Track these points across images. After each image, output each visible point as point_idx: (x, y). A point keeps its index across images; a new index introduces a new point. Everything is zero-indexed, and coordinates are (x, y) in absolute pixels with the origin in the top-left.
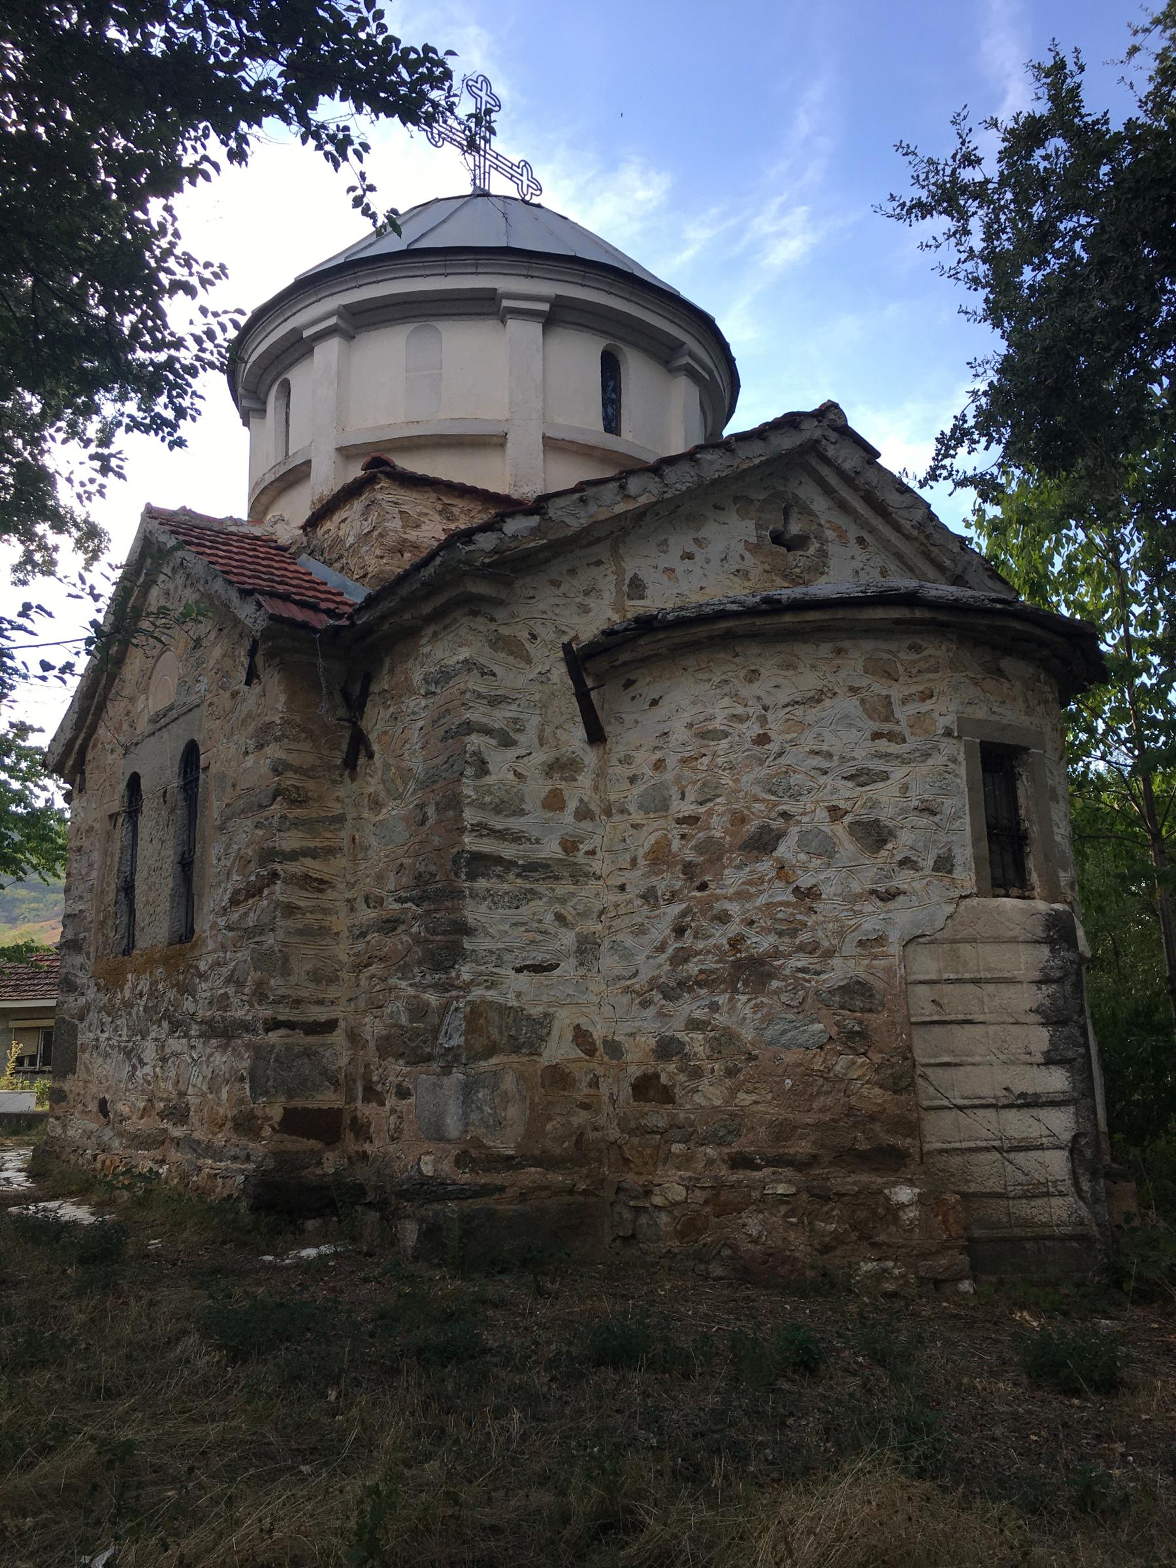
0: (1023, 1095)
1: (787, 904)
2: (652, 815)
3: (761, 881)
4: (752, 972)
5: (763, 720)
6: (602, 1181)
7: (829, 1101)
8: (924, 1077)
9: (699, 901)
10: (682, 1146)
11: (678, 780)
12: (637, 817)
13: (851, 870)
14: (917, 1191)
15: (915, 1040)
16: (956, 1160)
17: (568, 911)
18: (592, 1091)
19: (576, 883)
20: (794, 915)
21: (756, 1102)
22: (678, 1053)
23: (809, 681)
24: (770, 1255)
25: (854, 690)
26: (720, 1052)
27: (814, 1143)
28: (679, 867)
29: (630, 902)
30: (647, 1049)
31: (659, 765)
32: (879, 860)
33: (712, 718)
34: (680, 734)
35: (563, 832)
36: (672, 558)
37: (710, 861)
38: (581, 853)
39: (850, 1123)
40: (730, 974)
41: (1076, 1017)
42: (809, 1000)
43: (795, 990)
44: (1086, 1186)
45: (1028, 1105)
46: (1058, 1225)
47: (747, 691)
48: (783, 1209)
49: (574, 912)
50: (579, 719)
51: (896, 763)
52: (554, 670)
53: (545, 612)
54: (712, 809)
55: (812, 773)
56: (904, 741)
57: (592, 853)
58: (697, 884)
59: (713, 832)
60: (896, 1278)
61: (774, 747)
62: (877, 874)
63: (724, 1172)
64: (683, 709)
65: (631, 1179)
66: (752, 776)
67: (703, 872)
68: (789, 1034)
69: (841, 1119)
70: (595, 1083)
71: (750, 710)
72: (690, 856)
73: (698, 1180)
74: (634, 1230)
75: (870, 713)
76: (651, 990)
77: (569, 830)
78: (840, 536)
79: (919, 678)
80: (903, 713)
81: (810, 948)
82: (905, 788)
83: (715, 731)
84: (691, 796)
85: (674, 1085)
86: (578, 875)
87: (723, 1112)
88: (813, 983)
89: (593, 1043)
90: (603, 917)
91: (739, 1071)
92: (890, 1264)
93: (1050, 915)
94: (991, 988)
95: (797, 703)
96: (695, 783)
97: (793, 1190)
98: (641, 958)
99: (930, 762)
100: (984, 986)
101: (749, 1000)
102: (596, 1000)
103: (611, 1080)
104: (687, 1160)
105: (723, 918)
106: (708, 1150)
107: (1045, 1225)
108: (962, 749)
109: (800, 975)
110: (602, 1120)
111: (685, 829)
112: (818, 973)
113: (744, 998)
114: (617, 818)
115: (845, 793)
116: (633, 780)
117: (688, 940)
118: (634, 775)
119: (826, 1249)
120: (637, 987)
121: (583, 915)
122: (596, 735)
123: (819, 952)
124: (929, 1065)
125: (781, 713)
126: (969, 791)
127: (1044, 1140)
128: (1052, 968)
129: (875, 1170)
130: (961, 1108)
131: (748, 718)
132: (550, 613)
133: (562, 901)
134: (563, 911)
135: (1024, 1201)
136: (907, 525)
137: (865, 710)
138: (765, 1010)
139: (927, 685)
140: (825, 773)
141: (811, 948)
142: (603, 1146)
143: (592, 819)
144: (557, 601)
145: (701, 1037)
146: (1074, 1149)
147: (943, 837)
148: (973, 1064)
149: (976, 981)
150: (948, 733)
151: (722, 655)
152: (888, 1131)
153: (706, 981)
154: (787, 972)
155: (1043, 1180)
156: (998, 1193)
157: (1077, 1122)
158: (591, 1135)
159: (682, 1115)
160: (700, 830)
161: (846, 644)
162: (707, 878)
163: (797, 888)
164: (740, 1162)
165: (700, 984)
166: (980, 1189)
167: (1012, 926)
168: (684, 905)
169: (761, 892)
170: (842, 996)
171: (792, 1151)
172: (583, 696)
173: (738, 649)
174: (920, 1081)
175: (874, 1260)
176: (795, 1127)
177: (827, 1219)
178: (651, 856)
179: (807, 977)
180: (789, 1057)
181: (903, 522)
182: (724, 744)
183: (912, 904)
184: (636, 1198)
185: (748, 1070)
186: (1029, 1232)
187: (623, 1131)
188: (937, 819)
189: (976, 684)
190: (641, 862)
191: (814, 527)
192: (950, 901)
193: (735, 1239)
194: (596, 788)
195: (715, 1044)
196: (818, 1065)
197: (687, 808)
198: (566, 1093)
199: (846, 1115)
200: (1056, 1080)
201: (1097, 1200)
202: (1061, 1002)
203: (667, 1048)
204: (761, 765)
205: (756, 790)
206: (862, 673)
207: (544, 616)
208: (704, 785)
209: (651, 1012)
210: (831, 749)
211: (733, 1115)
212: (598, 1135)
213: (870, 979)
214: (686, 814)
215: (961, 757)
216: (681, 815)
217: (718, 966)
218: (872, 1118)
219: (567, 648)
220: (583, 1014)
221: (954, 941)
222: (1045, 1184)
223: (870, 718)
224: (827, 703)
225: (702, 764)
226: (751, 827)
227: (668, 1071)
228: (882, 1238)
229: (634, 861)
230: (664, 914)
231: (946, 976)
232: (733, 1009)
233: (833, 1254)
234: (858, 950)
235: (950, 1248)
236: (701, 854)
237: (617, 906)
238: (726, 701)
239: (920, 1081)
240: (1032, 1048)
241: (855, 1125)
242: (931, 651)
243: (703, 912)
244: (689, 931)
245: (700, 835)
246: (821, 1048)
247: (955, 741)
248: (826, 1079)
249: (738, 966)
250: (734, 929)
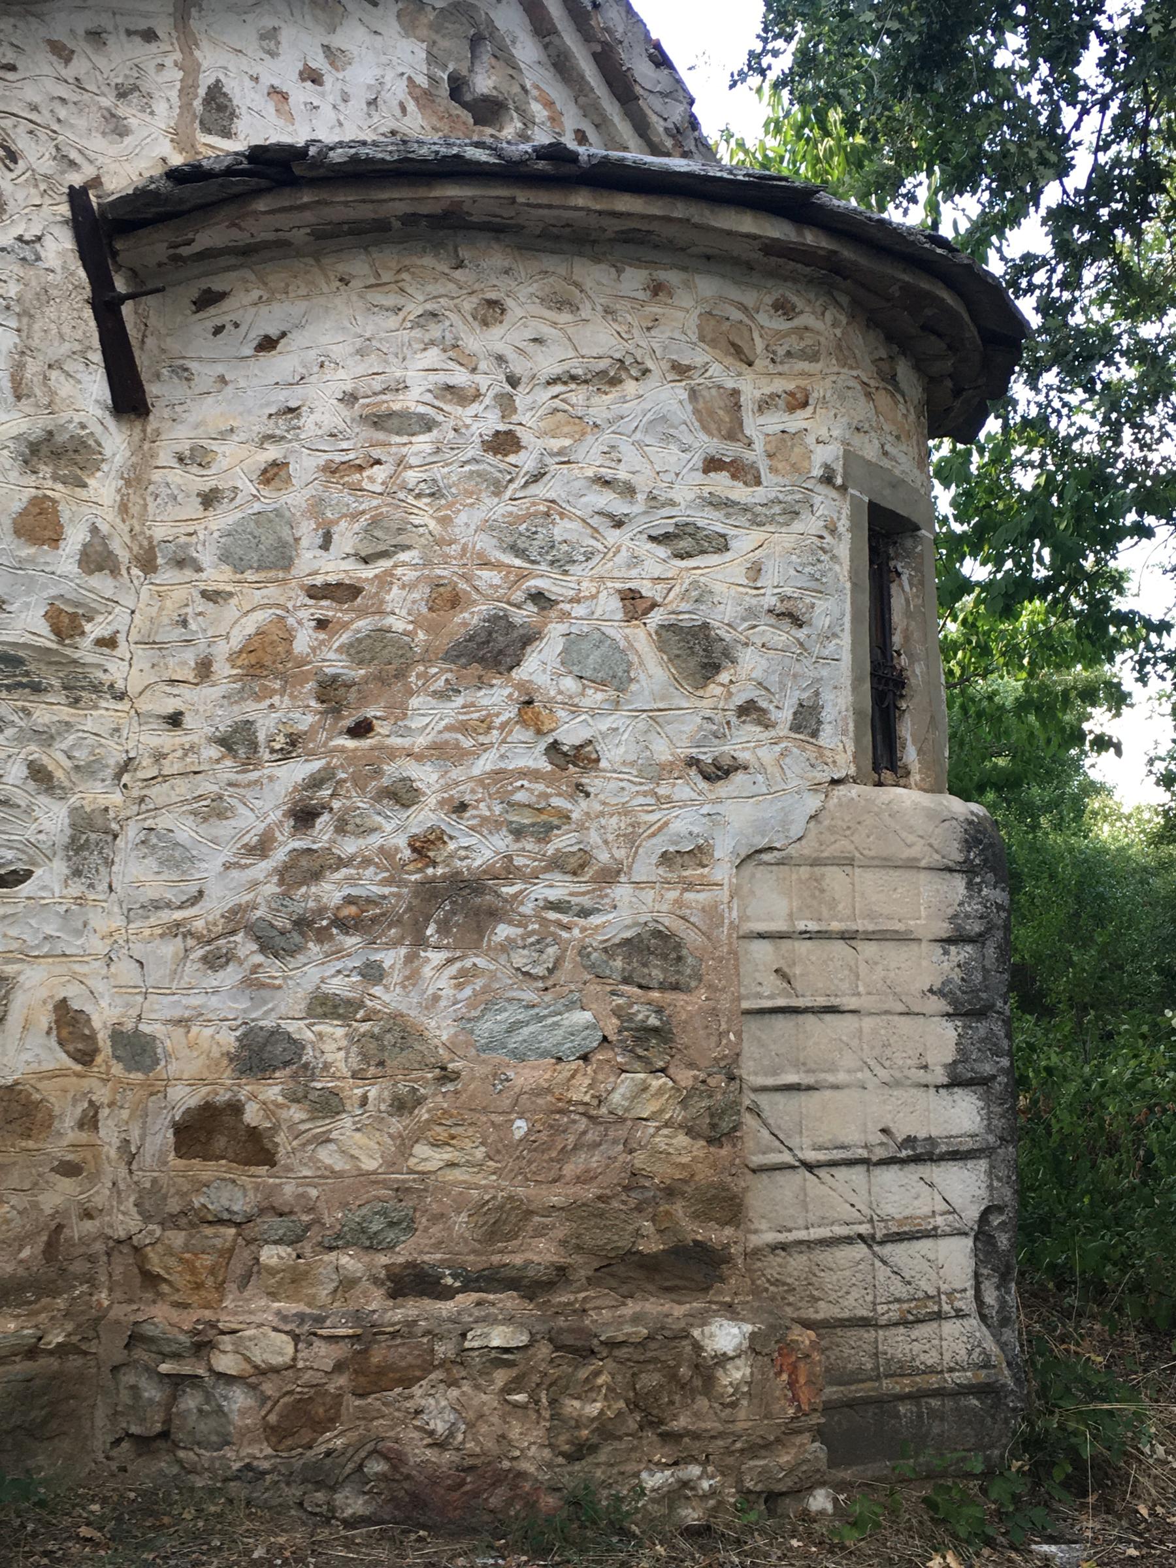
0: (910, 1141)
1: (534, 775)
2: (250, 576)
3: (486, 724)
4: (458, 904)
5: (506, 404)
6: (97, 1320)
7: (595, 1160)
8: (755, 1111)
9: (351, 758)
10: (284, 1251)
11: (316, 507)
12: (217, 576)
13: (655, 717)
14: (748, 1328)
15: (745, 1045)
16: (797, 1263)
17: (56, 760)
18: (84, 1137)
19: (75, 702)
20: (546, 796)
21: (452, 1165)
22: (287, 1064)
23: (600, 340)
24: (471, 1469)
25: (681, 370)
26: (381, 1064)
27: (563, 1243)
28: (310, 685)
29: (192, 749)
30: (215, 1053)
31: (273, 473)
32: (706, 703)
33: (401, 387)
34: (324, 412)
35: (53, 592)
36: (282, 71)
37: (382, 680)
38: (87, 643)
39: (632, 1203)
40: (410, 909)
41: (999, 1004)
42: (567, 965)
43: (540, 945)
44: (990, 1297)
45: (916, 1159)
46: (951, 1370)
47: (475, 341)
48: (501, 1377)
49: (67, 764)
50: (97, 357)
51: (743, 520)
52: (48, 241)
53: (35, 108)
54: (388, 573)
55: (595, 521)
56: (758, 483)
57: (109, 643)
58: (349, 722)
59: (390, 620)
60: (704, 1497)
61: (526, 461)
62: (701, 728)
63: (375, 1301)
64: (326, 366)
65: (162, 1317)
66: (478, 516)
67: (364, 700)
68: (526, 1031)
69: (614, 1196)
70: (90, 1121)
71: (483, 381)
72: (335, 664)
73: (319, 1320)
74: (168, 1421)
75: (705, 419)
76: (233, 932)
77: (67, 588)
78: (552, 119)
79: (785, 368)
80: (760, 427)
81: (573, 862)
82: (756, 570)
83: (404, 415)
84: (346, 538)
85: (275, 1129)
86: (81, 688)
87: (385, 1184)
88: (576, 932)
89: (92, 1038)
90: (126, 778)
91: (419, 1101)
92: (695, 1470)
93: (971, 823)
94: (869, 949)
95: (573, 378)
96: (355, 516)
97: (524, 1339)
98: (211, 866)
99: (798, 526)
100: (860, 945)
101: (450, 961)
102: (102, 947)
103: (125, 1114)
104: (295, 1280)
105: (403, 795)
106: (344, 1260)
107: (931, 1370)
108: (846, 511)
109: (552, 915)
110: (101, 1195)
111: (326, 609)
112: (585, 913)
113: (436, 957)
114: (167, 575)
115: (653, 567)
116: (209, 499)
117: (323, 832)
118: (215, 490)
119: (580, 1452)
120: (199, 925)
121: (86, 770)
122: (129, 400)
123: (589, 872)
124: (764, 1089)
125: (544, 395)
126: (853, 591)
127: (939, 1221)
128: (967, 916)
129: (668, 1289)
130: (810, 1167)
131: (477, 396)
132: (45, 112)
133: (46, 737)
134: (45, 760)
135: (901, 1330)
136: (659, 126)
137: (696, 411)
138: (479, 983)
139: (803, 383)
140: (619, 524)
141: (574, 865)
142: (99, 1247)
143: (115, 572)
144: (62, 91)
145: (340, 1032)
146: (983, 1235)
147: (806, 668)
148: (836, 1087)
149: (847, 937)
150: (828, 479)
151: (428, 261)
152: (695, 1216)
153: (358, 919)
154: (528, 909)
155: (932, 1292)
156: (863, 1319)
157: (990, 1187)
158: (80, 1229)
159: (289, 1189)
160: (363, 613)
161: (671, 277)
162: (371, 712)
163: (554, 747)
164: (412, 1282)
165: (343, 925)
166: (837, 1312)
167: (911, 838)
168: (317, 765)
169: (485, 747)
170: (628, 958)
171: (518, 1260)
172: (106, 308)
173: (464, 253)
174: (749, 1120)
175: (667, 1465)
176: (530, 1213)
177: (587, 1391)
178: (244, 660)
179: (565, 919)
180: (525, 1077)
181: (654, 118)
182: (423, 443)
183: (755, 789)
184: (176, 1356)
185: (437, 1100)
186: (905, 1385)
187: (147, 1218)
188: (801, 634)
189: (868, 395)
190: (222, 669)
191: (516, 89)
192: (815, 787)
193: (397, 1440)
194: (123, 509)
195: (373, 1046)
196: (580, 1092)
197: (333, 567)
198: (31, 1144)
199: (627, 1189)
200: (962, 1115)
201: (1005, 1321)
202: (978, 977)
203: (260, 1053)
204: (497, 494)
205: (485, 543)
206: (694, 338)
207: (33, 116)
208: (375, 522)
209: (230, 976)
210: (635, 480)
211: (401, 1191)
212: (89, 1226)
213: (676, 925)
214: (332, 579)
215: (843, 525)
216: (319, 580)
217: (386, 891)
218: (670, 1192)
219: (77, 197)
220: (74, 976)
221: (816, 863)
222: (936, 1298)
223: (705, 429)
224: (630, 387)
225: (371, 479)
226: (472, 616)
227: (261, 1100)
228: (682, 1422)
229: (204, 669)
230: (271, 778)
231: (801, 926)
232: (413, 978)
233: (590, 1459)
234: (661, 871)
235: (798, 1432)
236: (361, 662)
237: (159, 757)
238: (433, 357)
239: (749, 1120)
240: (930, 1059)
241: (639, 1209)
242: (806, 319)
243: (359, 782)
244: (325, 817)
245: (360, 623)
246: (585, 1058)
247: (834, 494)
248: (590, 1118)
249: (429, 893)
250: (422, 818)
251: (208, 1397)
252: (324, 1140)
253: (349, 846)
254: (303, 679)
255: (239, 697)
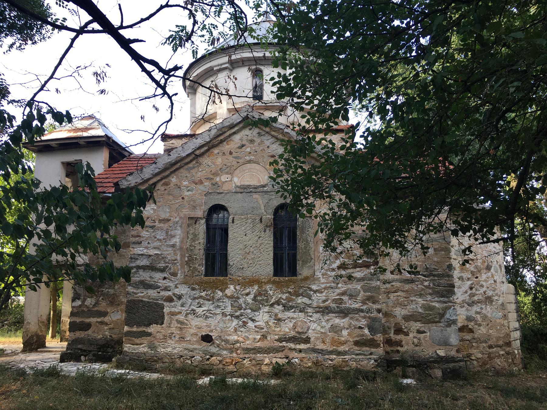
9: (476, 281)
67: (477, 274)
105: (482, 286)
153: (479, 302)
164: (491, 347)
203: (469, 319)
209: (464, 309)
211: (489, 335)
227: (471, 325)
232: (486, 309)
251: (470, 362)
252: (480, 329)
253: (478, 292)
254: (469, 271)
255: (461, 273)
